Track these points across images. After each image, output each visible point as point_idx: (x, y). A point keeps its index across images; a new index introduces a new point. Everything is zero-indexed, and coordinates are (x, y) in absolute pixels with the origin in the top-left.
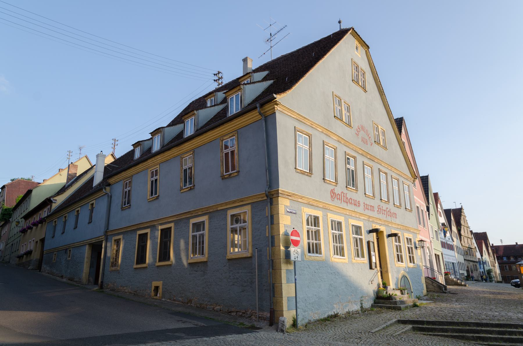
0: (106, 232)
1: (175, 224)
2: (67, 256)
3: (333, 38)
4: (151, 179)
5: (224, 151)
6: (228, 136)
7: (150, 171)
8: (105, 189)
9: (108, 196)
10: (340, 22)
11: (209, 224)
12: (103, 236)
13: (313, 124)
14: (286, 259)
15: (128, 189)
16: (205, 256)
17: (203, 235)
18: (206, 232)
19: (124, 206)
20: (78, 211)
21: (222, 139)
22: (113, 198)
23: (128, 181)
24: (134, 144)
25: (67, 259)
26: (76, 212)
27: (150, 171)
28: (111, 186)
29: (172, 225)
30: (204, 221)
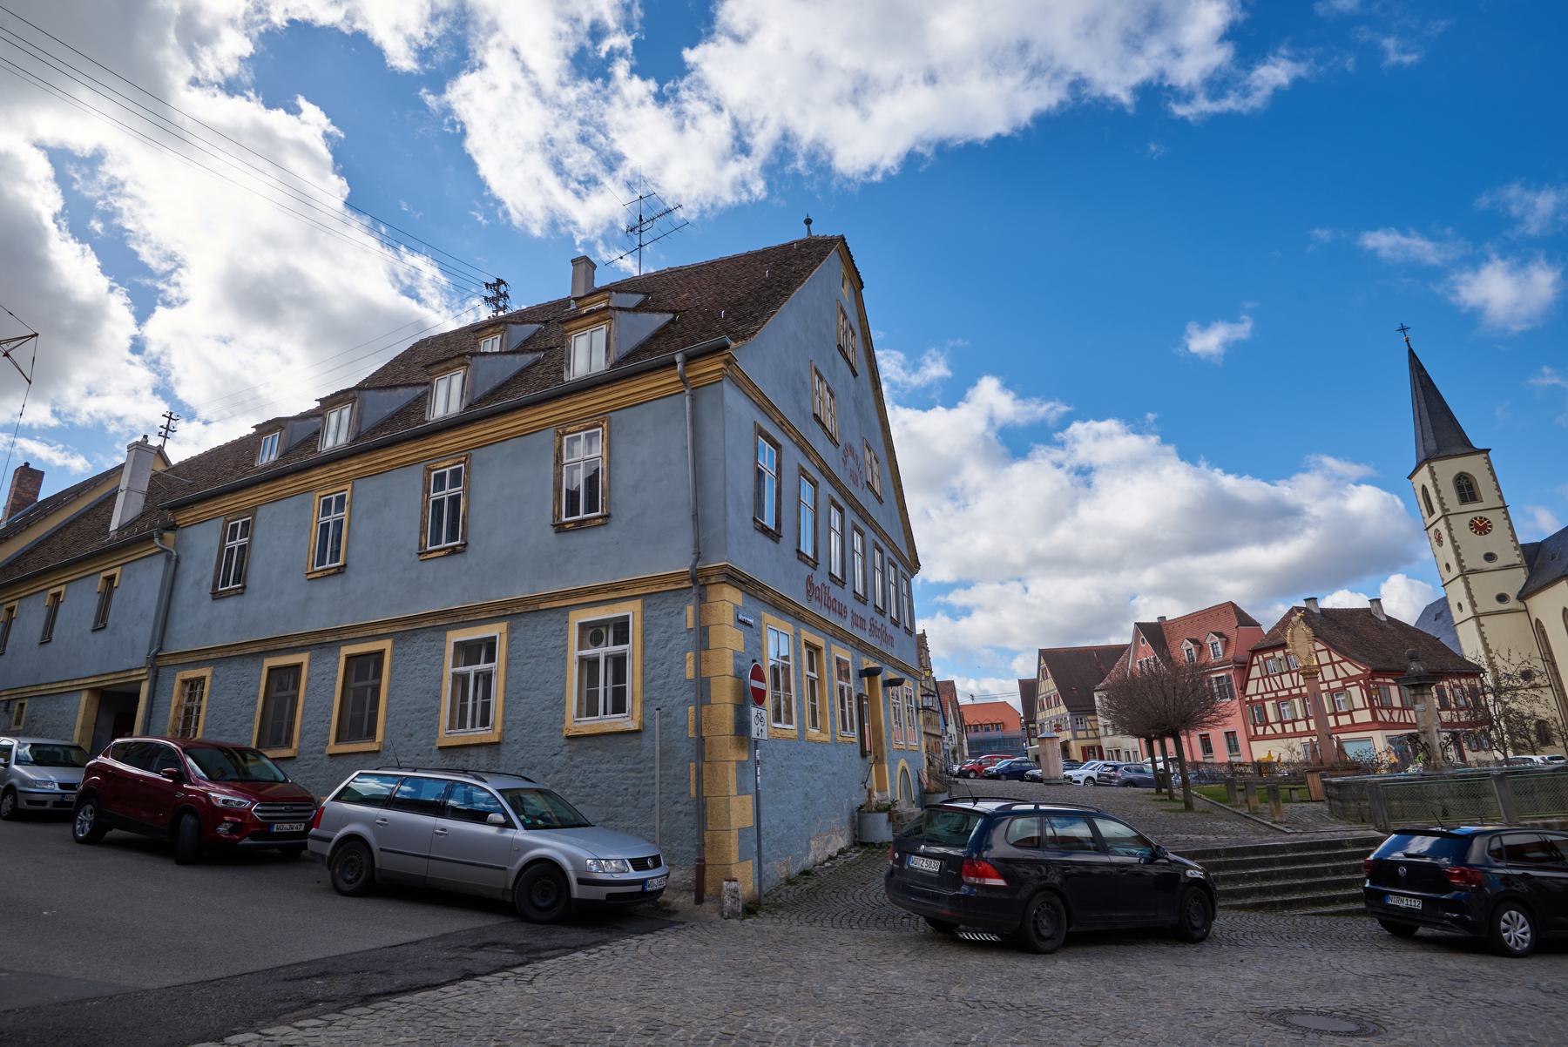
0: (156, 657)
1: (394, 643)
2: (11, 718)
3: (798, 249)
4: (321, 519)
5: (432, 495)
6: (582, 426)
7: (321, 497)
8: (161, 538)
9: (168, 558)
10: (808, 222)
11: (509, 645)
12: (144, 668)
13: (784, 422)
14: (735, 735)
15: (239, 541)
16: (493, 728)
17: (486, 678)
18: (498, 666)
19: (220, 589)
20: (57, 595)
21: (560, 431)
22: (182, 566)
23: (240, 521)
24: (296, 413)
25: (10, 727)
26: (101, 579)
27: (321, 497)
28: (178, 531)
29: (386, 645)
30: (495, 637)
